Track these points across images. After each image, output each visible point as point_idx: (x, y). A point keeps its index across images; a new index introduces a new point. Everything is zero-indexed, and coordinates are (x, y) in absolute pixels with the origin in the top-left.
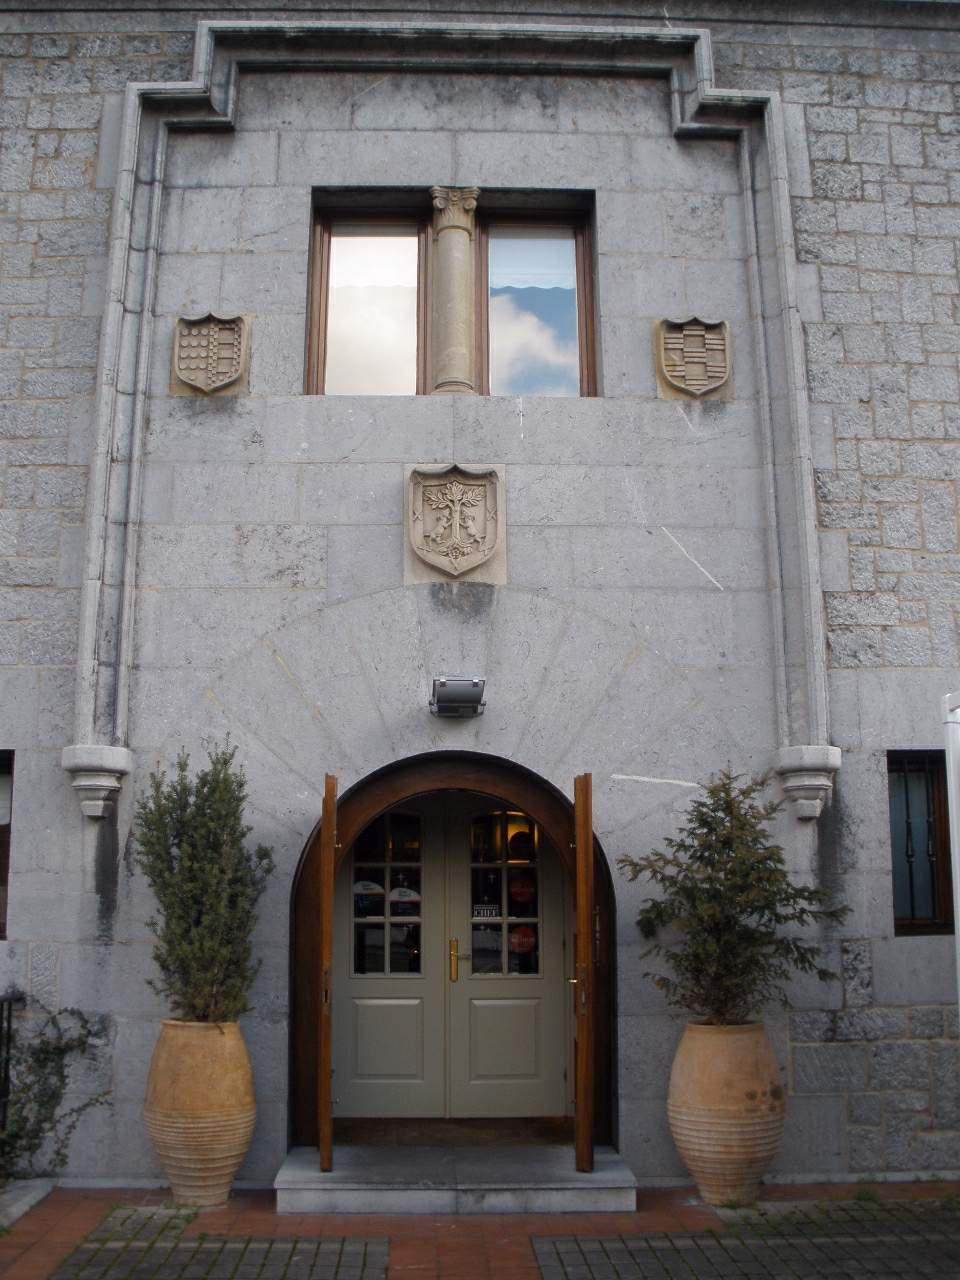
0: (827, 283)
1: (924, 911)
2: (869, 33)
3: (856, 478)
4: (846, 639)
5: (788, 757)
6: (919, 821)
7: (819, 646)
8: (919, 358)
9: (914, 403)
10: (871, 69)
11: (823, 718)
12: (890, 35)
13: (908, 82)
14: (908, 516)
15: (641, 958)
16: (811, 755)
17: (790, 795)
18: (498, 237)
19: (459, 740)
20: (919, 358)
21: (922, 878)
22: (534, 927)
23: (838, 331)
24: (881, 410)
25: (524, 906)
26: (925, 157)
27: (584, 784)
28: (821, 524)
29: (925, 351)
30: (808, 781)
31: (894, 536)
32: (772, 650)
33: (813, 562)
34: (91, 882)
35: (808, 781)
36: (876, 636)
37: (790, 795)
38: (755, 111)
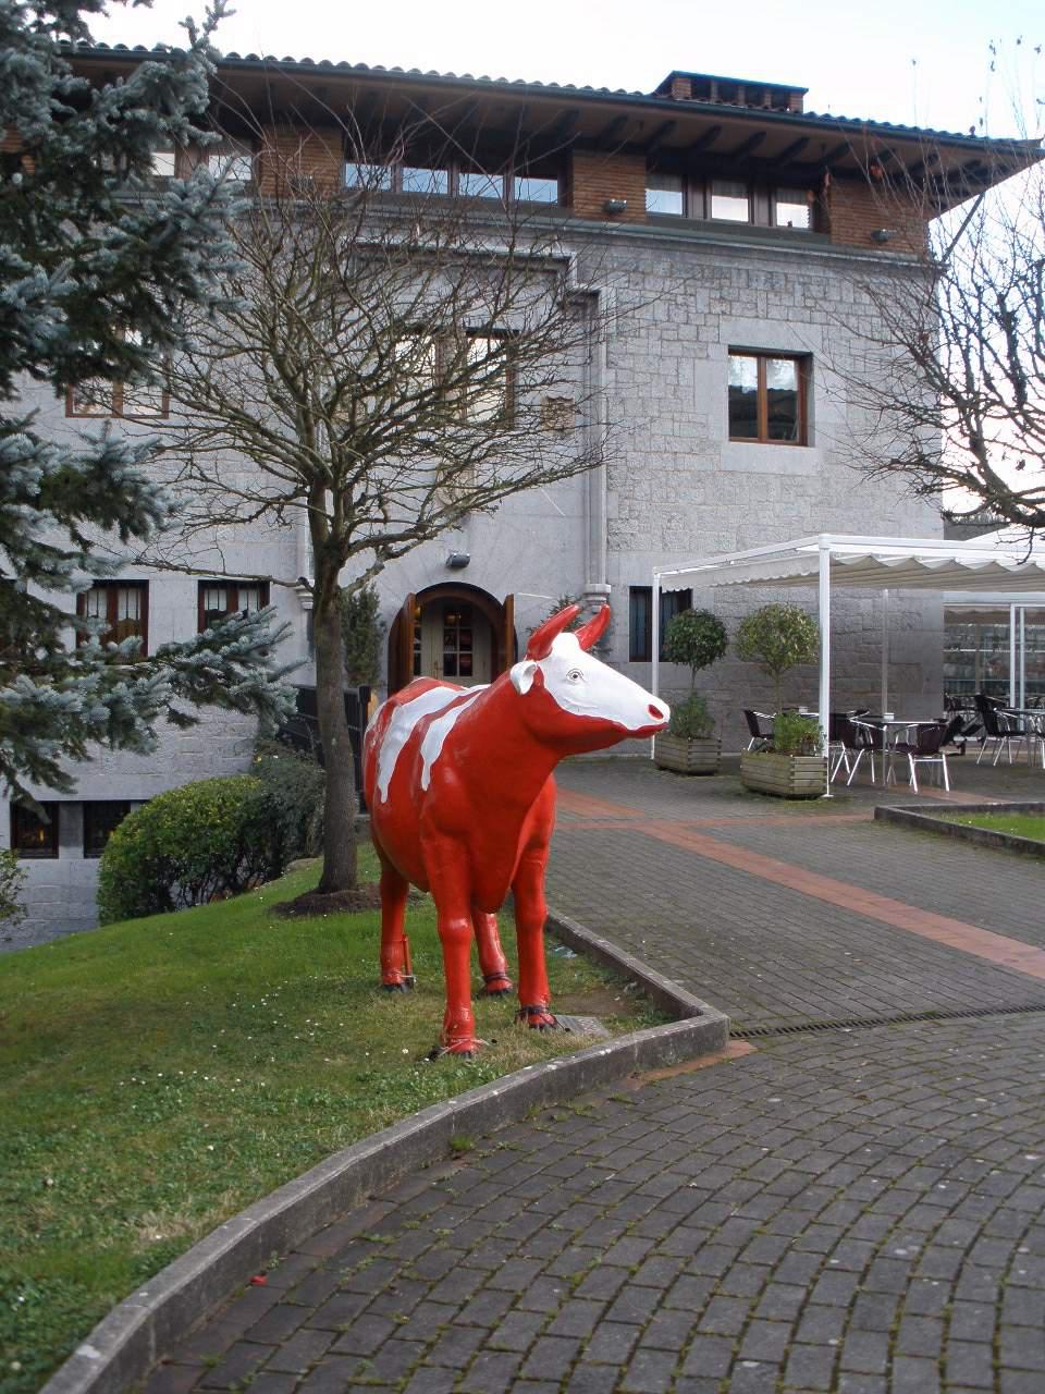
0: (620, 379)
1: (641, 652)
2: (649, 251)
3: (625, 469)
4: (616, 538)
5: (589, 588)
6: (642, 614)
7: (604, 543)
8: (656, 414)
9: (653, 435)
10: (649, 270)
11: (604, 572)
12: (658, 252)
13: (664, 278)
14: (645, 486)
15: (290, 623)
16: (598, 587)
17: (590, 603)
18: (724, 194)
19: (456, 577)
20: (656, 414)
21: (641, 634)
22: (471, 656)
23: (622, 401)
24: (638, 439)
25: (466, 646)
26: (669, 316)
27: (510, 599)
28: (608, 488)
29: (659, 411)
30: (597, 598)
31: (638, 494)
32: (584, 542)
33: (604, 508)
34: (305, 636)
35: (597, 598)
36: (628, 538)
37: (590, 603)
38: (595, 295)
